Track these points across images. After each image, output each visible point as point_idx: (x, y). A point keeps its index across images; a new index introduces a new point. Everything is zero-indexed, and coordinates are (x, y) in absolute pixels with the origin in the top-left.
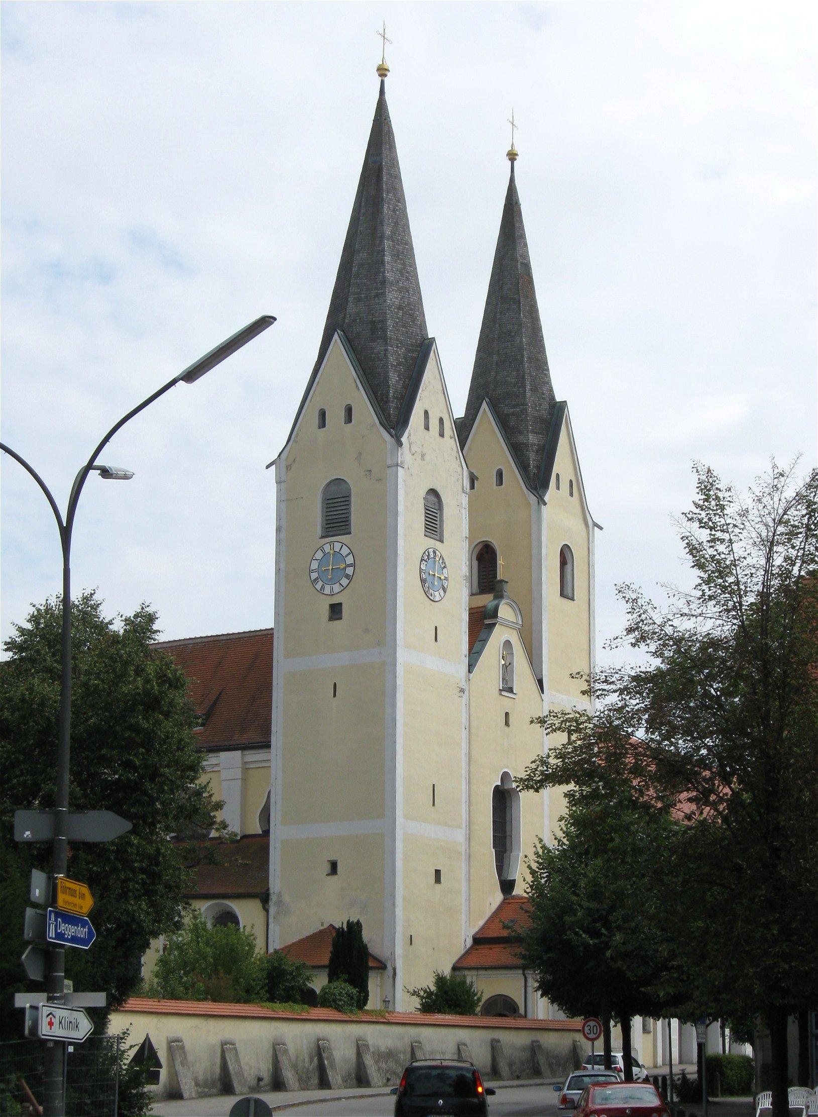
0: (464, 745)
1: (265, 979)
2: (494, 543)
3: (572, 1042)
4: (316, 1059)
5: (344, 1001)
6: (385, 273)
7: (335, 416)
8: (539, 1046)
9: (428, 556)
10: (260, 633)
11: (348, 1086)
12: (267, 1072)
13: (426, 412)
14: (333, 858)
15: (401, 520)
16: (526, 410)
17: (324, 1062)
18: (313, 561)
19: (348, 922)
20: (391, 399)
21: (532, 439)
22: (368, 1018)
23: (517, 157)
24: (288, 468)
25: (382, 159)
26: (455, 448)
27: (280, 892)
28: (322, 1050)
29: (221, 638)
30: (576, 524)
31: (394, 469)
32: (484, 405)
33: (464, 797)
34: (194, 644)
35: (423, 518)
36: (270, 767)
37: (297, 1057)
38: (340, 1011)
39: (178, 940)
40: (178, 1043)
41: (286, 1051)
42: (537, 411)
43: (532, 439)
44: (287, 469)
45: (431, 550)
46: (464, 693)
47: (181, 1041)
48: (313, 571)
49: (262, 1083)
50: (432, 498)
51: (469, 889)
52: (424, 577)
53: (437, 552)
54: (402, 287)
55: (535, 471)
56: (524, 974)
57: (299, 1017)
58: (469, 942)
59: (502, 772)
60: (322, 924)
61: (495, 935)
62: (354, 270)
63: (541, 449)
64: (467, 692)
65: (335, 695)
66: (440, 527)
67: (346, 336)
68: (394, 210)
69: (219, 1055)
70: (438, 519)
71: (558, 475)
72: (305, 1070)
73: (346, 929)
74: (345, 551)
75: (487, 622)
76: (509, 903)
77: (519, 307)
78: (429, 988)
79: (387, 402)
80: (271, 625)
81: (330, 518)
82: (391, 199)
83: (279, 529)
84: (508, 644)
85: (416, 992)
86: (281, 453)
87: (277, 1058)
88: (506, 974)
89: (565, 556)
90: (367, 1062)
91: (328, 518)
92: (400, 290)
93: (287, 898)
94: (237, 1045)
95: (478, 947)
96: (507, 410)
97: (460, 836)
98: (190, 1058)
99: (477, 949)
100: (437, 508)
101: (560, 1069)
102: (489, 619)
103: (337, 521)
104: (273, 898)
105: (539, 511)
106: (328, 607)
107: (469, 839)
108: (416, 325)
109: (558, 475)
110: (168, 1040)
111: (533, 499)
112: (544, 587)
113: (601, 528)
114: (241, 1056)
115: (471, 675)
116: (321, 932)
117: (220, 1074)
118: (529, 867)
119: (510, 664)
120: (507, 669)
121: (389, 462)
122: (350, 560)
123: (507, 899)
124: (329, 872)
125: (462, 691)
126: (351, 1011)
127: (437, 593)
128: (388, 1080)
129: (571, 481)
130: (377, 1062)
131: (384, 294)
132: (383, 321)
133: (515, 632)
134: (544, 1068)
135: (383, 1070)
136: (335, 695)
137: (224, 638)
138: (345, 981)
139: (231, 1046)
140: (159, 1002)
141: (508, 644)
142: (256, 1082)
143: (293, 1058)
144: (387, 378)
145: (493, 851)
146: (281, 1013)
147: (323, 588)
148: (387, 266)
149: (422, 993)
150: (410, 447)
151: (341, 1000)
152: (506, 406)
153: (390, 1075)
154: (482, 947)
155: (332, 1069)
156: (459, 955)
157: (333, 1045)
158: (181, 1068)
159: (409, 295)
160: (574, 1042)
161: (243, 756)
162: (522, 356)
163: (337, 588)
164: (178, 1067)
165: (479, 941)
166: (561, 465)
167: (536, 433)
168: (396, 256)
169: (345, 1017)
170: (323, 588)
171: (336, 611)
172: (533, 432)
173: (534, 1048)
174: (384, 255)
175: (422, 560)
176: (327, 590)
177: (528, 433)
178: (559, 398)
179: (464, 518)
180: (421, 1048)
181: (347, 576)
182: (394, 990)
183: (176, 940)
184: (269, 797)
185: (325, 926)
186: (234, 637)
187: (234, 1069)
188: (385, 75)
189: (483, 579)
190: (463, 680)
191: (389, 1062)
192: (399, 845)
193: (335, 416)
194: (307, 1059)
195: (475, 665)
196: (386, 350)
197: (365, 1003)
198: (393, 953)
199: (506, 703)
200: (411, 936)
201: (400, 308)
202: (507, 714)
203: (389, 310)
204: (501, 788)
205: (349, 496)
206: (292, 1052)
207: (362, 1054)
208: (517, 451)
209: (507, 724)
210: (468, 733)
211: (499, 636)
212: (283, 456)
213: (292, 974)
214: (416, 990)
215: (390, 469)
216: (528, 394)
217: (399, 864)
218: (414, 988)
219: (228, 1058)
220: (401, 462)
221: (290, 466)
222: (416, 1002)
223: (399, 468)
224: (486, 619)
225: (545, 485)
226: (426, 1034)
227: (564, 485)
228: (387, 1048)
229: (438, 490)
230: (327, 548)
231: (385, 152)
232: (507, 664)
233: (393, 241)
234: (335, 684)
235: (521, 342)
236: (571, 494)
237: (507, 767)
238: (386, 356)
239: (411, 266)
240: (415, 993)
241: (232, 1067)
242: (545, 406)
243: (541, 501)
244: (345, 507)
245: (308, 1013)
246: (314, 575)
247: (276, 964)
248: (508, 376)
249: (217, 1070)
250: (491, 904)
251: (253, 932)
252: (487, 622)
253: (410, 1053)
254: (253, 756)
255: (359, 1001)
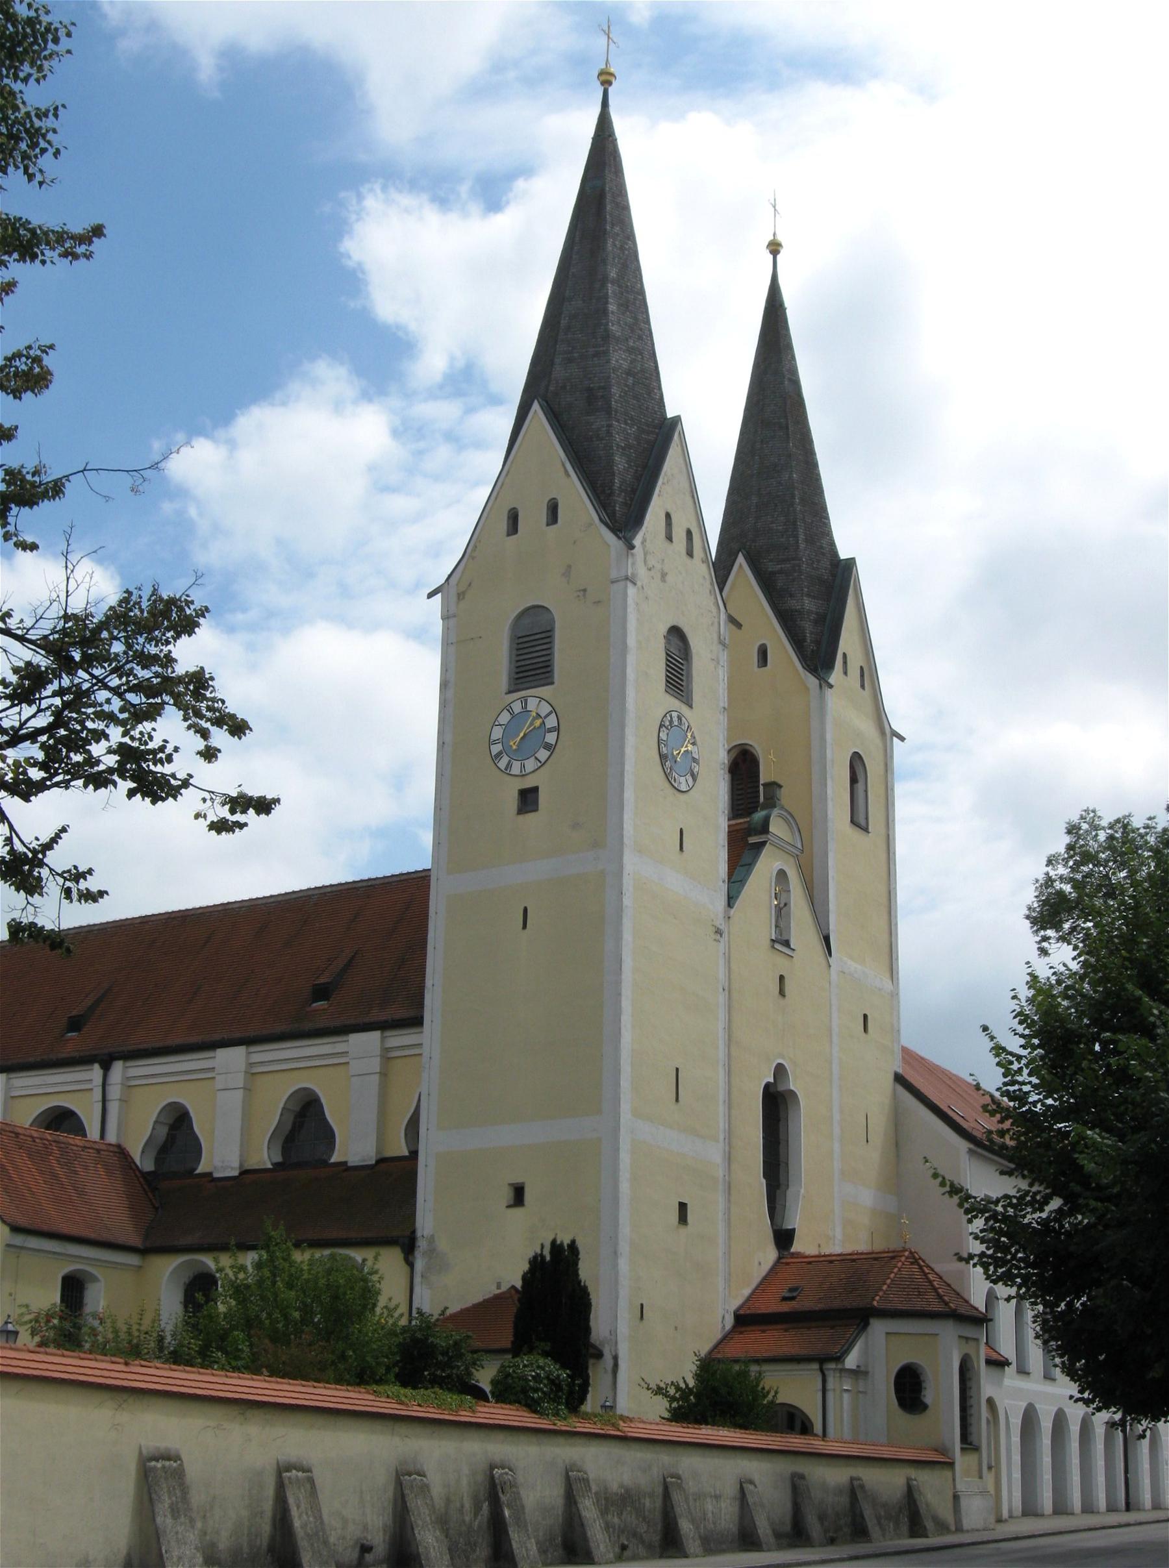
0: (722, 1014)
1: (393, 1354)
2: (756, 746)
3: (905, 1481)
4: (486, 1506)
5: (543, 1392)
6: (608, 325)
7: (533, 517)
8: (862, 1487)
9: (671, 721)
10: (415, 876)
11: (549, 1561)
12: (381, 1534)
13: (668, 516)
14: (518, 1180)
15: (631, 659)
16: (799, 566)
17: (502, 1511)
18: (495, 727)
19: (554, 1242)
20: (617, 492)
21: (808, 604)
22: (587, 1427)
23: (780, 248)
24: (461, 596)
25: (604, 184)
26: (707, 577)
27: (432, 1236)
28: (499, 1487)
29: (360, 885)
30: (867, 727)
31: (622, 584)
32: (741, 559)
33: (722, 1096)
34: (321, 894)
35: (664, 666)
36: (420, 1055)
37: (448, 1501)
38: (535, 1412)
39: (237, 1278)
40: (167, 1463)
41: (425, 1489)
42: (813, 569)
43: (808, 604)
44: (459, 598)
45: (674, 714)
46: (721, 936)
47: (177, 1458)
48: (495, 742)
49: (369, 1557)
50: (675, 640)
51: (729, 1238)
52: (664, 750)
53: (683, 719)
54: (633, 348)
55: (813, 647)
56: (822, 1371)
57: (451, 1418)
58: (729, 1322)
59: (774, 1065)
60: (499, 1286)
61: (770, 1311)
62: (564, 322)
63: (820, 619)
64: (725, 935)
65: (525, 926)
66: (688, 686)
67: (551, 408)
68: (622, 248)
69: (270, 1491)
70: (683, 678)
71: (845, 655)
72: (464, 1528)
73: (548, 1258)
74: (545, 709)
75: (753, 840)
76: (787, 1264)
77: (788, 434)
78: (685, 1382)
79: (611, 494)
80: (428, 865)
81: (523, 663)
82: (618, 235)
83: (444, 685)
84: (782, 875)
85: (662, 1389)
86: (450, 576)
87: (404, 1502)
88: (791, 1370)
89: (856, 764)
90: (584, 1513)
91: (520, 664)
92: (630, 350)
93: (442, 1245)
94: (317, 1473)
95: (743, 1329)
96: (772, 567)
97: (715, 1154)
98: (197, 1498)
99: (741, 1333)
100: (683, 657)
101: (891, 1525)
102: (755, 835)
103: (535, 666)
104: (422, 1244)
105: (822, 698)
106: (516, 794)
107: (729, 1158)
108: (653, 399)
109: (845, 655)
110: (140, 1453)
111: (812, 681)
112: (830, 804)
113: (902, 739)
114: (324, 1496)
115: (732, 911)
116: (497, 1298)
117: (273, 1538)
118: (998, 1050)
119: (785, 905)
120: (782, 912)
121: (614, 574)
122: (551, 722)
123: (783, 1258)
124: (512, 1202)
125: (719, 932)
126: (557, 1414)
127: (682, 779)
128: (624, 1548)
129: (862, 668)
130: (604, 1512)
131: (606, 353)
132: (606, 388)
133: (792, 859)
134: (871, 1523)
135: (614, 1529)
136: (525, 926)
137: (365, 884)
138: (546, 1354)
139: (300, 1474)
140: (126, 1364)
141: (782, 875)
142: (355, 1555)
143: (439, 1503)
144: (610, 463)
145: (764, 1181)
146: (416, 1408)
147: (509, 766)
148: (611, 317)
149: (672, 1391)
150: (645, 558)
151: (536, 1390)
152: (771, 561)
153: (628, 1539)
154: (748, 1329)
155: (519, 1527)
156: (714, 1341)
157: (520, 1479)
158: (169, 1521)
159: (642, 358)
160: (909, 1480)
161: (383, 1039)
162: (793, 496)
163: (530, 765)
164: (164, 1520)
165: (744, 1320)
166: (847, 642)
167: (814, 597)
168: (625, 306)
169: (543, 1423)
170: (509, 766)
171: (528, 799)
172: (808, 595)
173: (854, 1491)
174: (607, 303)
175: (661, 726)
176: (516, 769)
177: (802, 596)
178: (843, 554)
179: (721, 682)
180: (680, 1486)
181: (548, 746)
182: (615, 1393)
183: (233, 1278)
184: (419, 1100)
185: (504, 1288)
186: (378, 882)
187: (304, 1526)
188: (610, 83)
189: (738, 810)
190: (721, 915)
191: (624, 1513)
192: (625, 1158)
193: (533, 517)
194: (468, 1505)
195: (737, 897)
196: (610, 426)
197: (582, 1399)
198: (613, 1332)
199: (782, 964)
200: (642, 1305)
201: (629, 373)
202: (782, 978)
203: (613, 373)
204: (772, 1090)
205: (552, 630)
206: (437, 1491)
207: (577, 1497)
208: (788, 620)
209: (782, 993)
210: (727, 996)
211: (767, 865)
212: (453, 580)
213: (447, 1353)
214: (662, 1385)
215: (615, 584)
216: (802, 546)
217: (625, 1187)
218: (659, 1382)
219: (291, 1501)
220: (632, 574)
221: (464, 593)
222: (660, 1407)
223: (628, 582)
224: (750, 835)
225: (829, 665)
226: (690, 1464)
227: (854, 672)
228: (621, 1486)
229: (686, 630)
230: (517, 707)
231: (609, 176)
232: (782, 905)
233: (620, 286)
234: (525, 910)
235: (790, 478)
236: (863, 686)
237: (783, 1058)
238: (609, 433)
239: (642, 313)
240: (659, 1391)
241: (299, 1520)
242: (825, 563)
243: (824, 683)
244: (544, 647)
245: (473, 1412)
246: (496, 749)
247: (419, 1335)
248: (772, 522)
249: (266, 1527)
250: (760, 1264)
251: (376, 1267)
252: (753, 840)
253: (661, 1497)
254: (399, 1039)
255: (571, 1393)
